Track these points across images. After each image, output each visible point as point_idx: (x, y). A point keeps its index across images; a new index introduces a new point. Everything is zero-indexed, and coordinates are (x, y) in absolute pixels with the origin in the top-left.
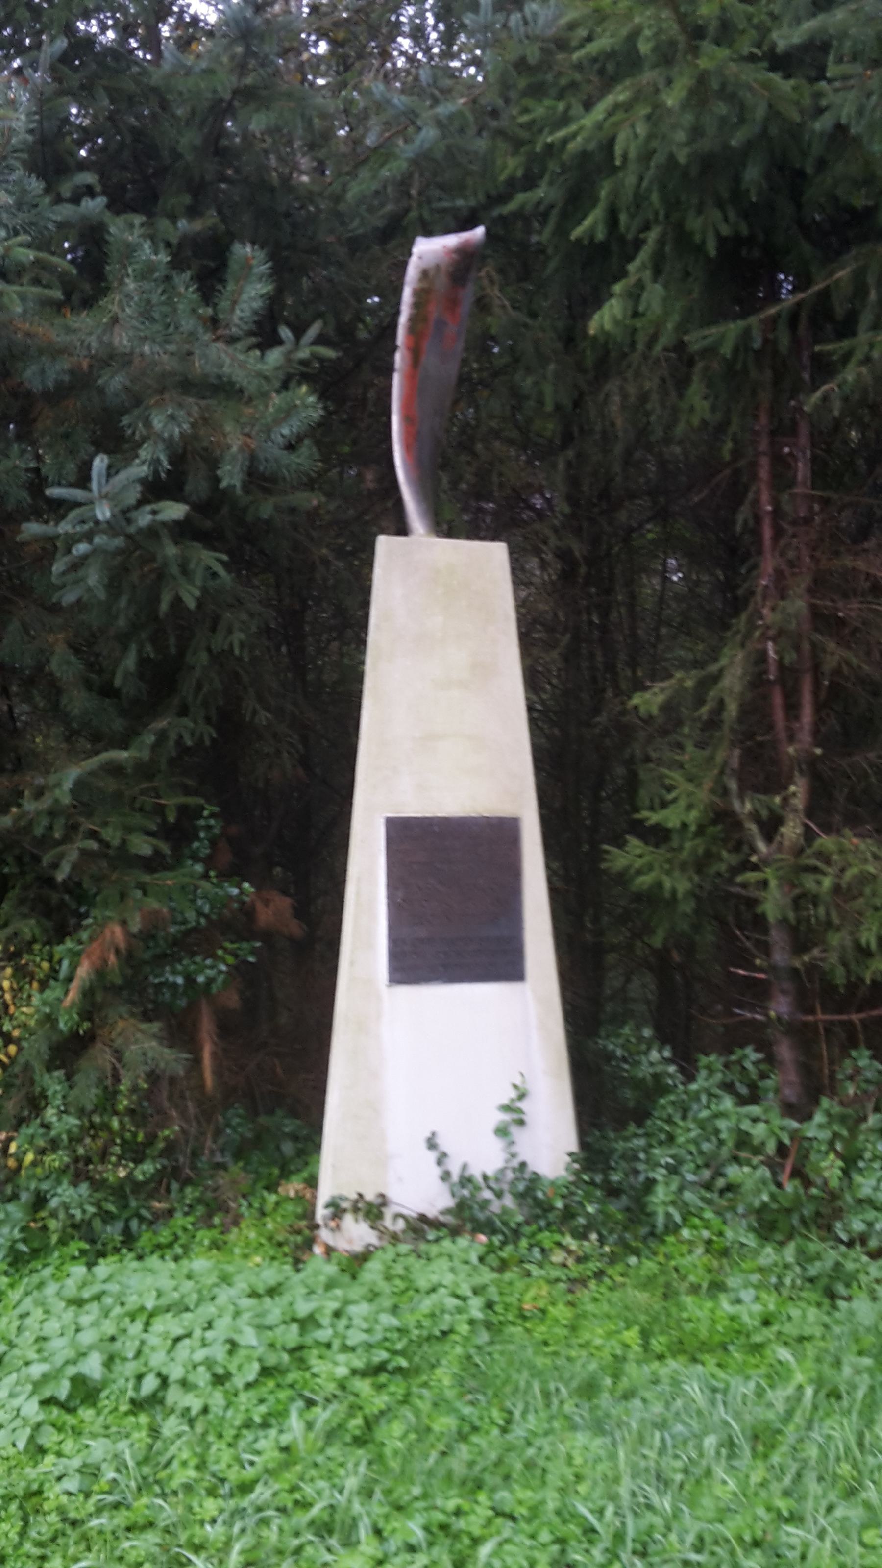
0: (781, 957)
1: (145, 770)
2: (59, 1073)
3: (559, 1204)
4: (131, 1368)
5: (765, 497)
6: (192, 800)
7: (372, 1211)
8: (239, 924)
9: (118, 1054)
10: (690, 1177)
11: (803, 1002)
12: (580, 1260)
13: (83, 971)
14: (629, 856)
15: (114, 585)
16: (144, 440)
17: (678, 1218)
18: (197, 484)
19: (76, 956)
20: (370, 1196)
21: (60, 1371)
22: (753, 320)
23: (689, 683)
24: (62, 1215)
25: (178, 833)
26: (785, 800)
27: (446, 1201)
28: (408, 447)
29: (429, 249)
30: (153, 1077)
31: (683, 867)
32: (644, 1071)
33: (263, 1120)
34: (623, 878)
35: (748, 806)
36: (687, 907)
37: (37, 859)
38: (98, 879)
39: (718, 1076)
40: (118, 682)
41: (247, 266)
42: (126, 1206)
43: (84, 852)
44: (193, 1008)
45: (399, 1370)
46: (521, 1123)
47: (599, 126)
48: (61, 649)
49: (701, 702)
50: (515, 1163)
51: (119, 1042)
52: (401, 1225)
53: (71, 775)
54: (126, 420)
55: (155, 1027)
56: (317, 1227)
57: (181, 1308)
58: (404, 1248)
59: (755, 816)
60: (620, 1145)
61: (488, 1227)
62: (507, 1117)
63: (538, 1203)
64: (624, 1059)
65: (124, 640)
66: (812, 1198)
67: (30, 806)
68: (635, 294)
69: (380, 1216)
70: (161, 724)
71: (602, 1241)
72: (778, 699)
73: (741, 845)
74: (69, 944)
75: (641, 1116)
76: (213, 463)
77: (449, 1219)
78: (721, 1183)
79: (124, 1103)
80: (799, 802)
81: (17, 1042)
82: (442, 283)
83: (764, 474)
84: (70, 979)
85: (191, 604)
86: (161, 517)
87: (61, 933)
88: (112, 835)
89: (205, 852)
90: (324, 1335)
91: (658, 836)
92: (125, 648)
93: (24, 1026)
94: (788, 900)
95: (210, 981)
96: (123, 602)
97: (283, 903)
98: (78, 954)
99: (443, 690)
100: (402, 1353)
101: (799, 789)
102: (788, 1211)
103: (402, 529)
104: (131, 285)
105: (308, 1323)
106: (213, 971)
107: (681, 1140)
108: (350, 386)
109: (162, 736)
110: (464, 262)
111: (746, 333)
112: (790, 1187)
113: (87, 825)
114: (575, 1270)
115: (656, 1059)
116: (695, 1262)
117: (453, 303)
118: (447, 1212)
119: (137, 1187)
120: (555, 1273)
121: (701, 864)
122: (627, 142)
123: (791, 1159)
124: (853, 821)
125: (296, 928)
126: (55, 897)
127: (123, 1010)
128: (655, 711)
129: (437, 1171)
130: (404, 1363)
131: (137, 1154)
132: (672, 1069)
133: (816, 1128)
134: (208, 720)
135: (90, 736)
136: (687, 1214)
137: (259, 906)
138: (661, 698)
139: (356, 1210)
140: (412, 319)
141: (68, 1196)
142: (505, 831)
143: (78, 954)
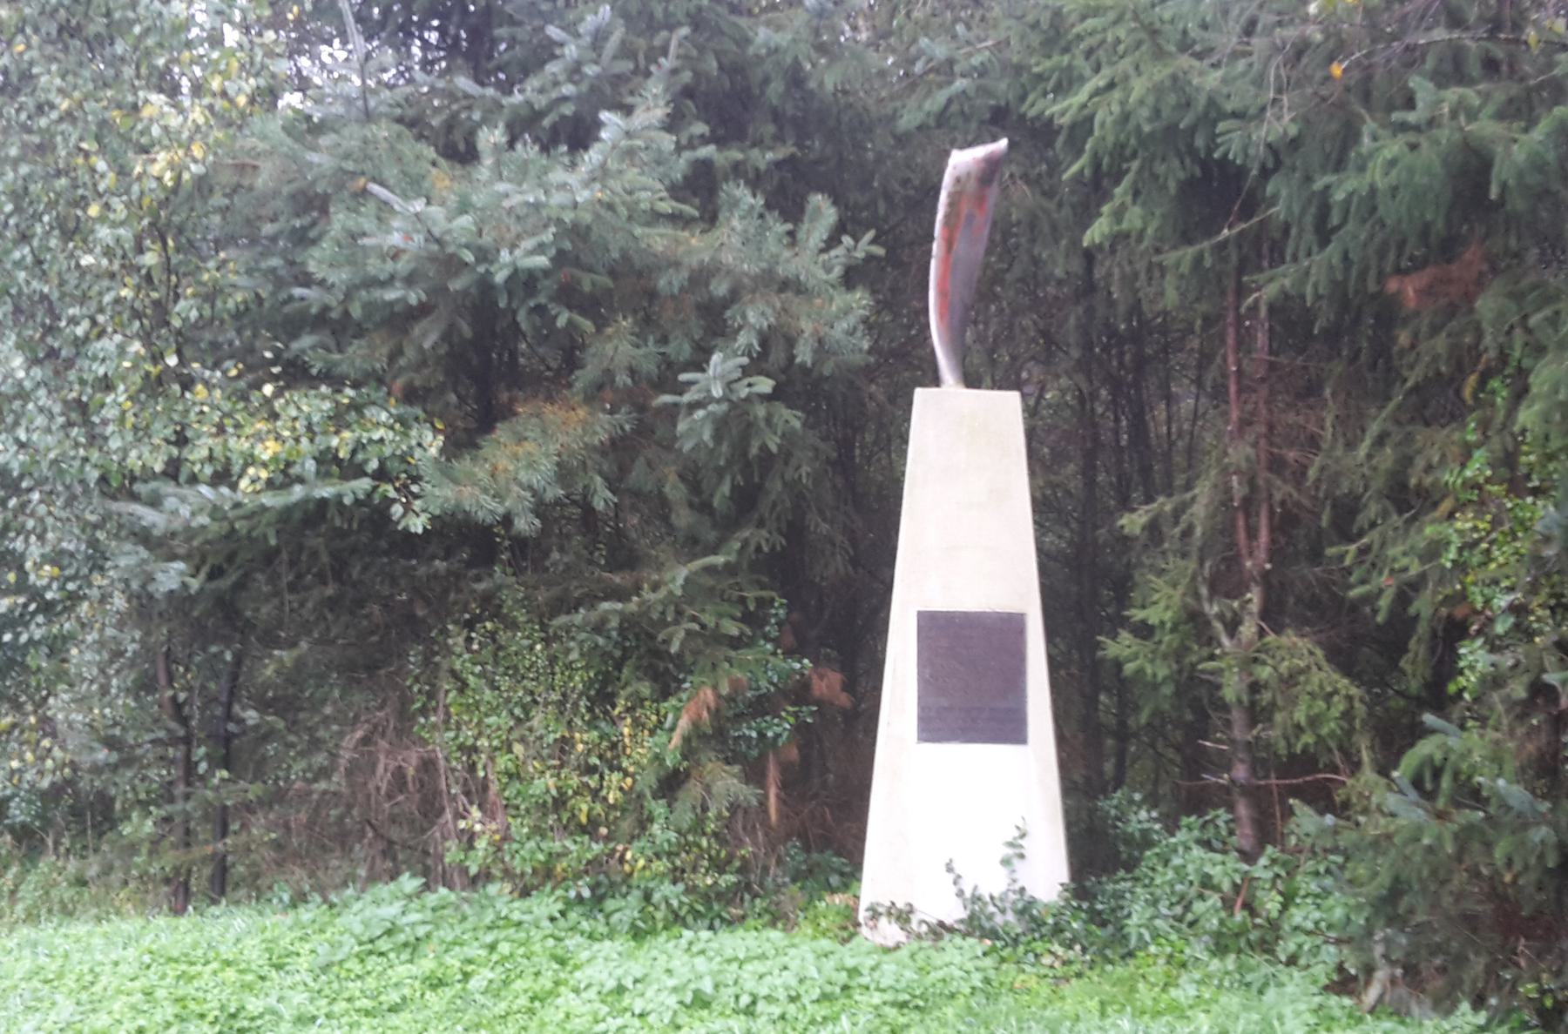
0: (1238, 733)
2: (662, 802)
3: (1050, 921)
4: (732, 991)
5: (1231, 359)
6: (764, 593)
7: (902, 917)
8: (800, 692)
9: (708, 788)
10: (1164, 911)
12: (1064, 963)
13: (684, 723)
14: (1119, 646)
15: (718, 437)
16: (740, 328)
17: (1147, 937)
18: (777, 356)
19: (678, 710)
20: (900, 905)
23: (1168, 508)
26: (1242, 607)
27: (964, 915)
28: (941, 316)
29: (963, 160)
30: (734, 808)
31: (1165, 657)
32: (1133, 827)
33: (815, 856)
34: (1118, 664)
35: (1216, 609)
36: (1168, 690)
37: (652, 637)
39: (1196, 833)
40: (716, 503)
41: (818, 210)
42: (710, 908)
44: (763, 757)
45: (917, 1007)
47: (1084, 106)
48: (673, 478)
50: (1017, 887)
51: (708, 779)
52: (924, 928)
54: (728, 313)
55: (736, 769)
57: (763, 957)
58: (926, 944)
59: (1221, 617)
60: (1110, 887)
61: (993, 934)
62: (1010, 851)
63: (1033, 919)
65: (720, 473)
66: (1256, 926)
68: (1118, 215)
69: (908, 920)
70: (746, 533)
71: (1084, 950)
72: (1241, 523)
73: (1212, 641)
74: (673, 701)
75: (1131, 865)
76: (791, 342)
78: (1190, 917)
79: (711, 827)
80: (1255, 607)
81: (632, 776)
82: (972, 186)
83: (1230, 340)
84: (672, 729)
85: (774, 449)
86: (756, 389)
87: (665, 694)
88: (709, 619)
90: (865, 980)
91: (1144, 631)
93: (636, 763)
94: (1244, 686)
95: (778, 736)
99: (967, 510)
100: (921, 997)
101: (1254, 596)
102: (1237, 935)
103: (936, 381)
104: (735, 223)
105: (854, 972)
106: (780, 727)
108: (892, 278)
110: (991, 168)
112: (1240, 916)
113: (690, 612)
115: (1142, 818)
116: (1159, 970)
117: (980, 200)
118: (962, 921)
119: (720, 896)
120: (1043, 971)
121: (1180, 654)
123: (1242, 896)
124: (1301, 623)
125: (844, 700)
126: (661, 666)
127: (712, 755)
128: (1137, 531)
129: (954, 889)
131: (720, 867)
132: (1157, 827)
133: (1261, 870)
135: (693, 546)
136: (1156, 935)
137: (815, 680)
139: (889, 914)
140: (947, 217)
141: (668, 891)
142: (1013, 625)
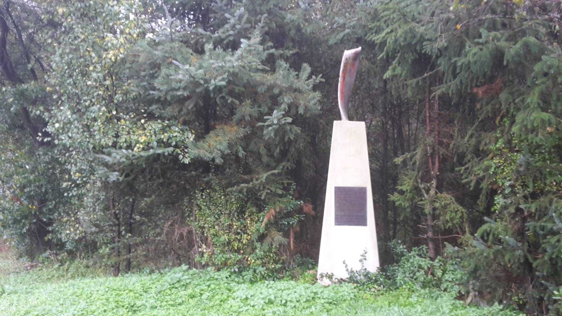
0: (429, 223)
1: (279, 174)
2: (259, 243)
3: (374, 278)
4: (280, 299)
5: (427, 112)
6: (290, 181)
7: (330, 277)
8: (300, 211)
9: (273, 239)
10: (408, 275)
11: (435, 232)
13: (266, 220)
14: (394, 197)
15: (276, 135)
16: (282, 103)
17: (402, 283)
18: (293, 111)
20: (329, 273)
21: (266, 297)
22: (420, 78)
23: (409, 156)
24: (259, 274)
25: (286, 189)
28: (342, 99)
29: (348, 53)
30: (280, 245)
31: (408, 200)
34: (394, 202)
37: (256, 194)
38: (269, 199)
40: (275, 155)
42: (273, 274)
43: (267, 193)
44: (289, 230)
45: (334, 304)
46: (365, 259)
47: (384, 37)
48: (262, 147)
49: (411, 161)
50: (364, 268)
51: (273, 236)
52: (337, 280)
53: (265, 175)
54: (279, 99)
55: (281, 233)
56: (317, 279)
57: (289, 289)
58: (337, 285)
59: (424, 188)
60: (391, 268)
61: (357, 282)
62: (362, 258)
63: (369, 278)
64: (394, 248)
65: (276, 146)
66: (435, 280)
67: (255, 182)
68: (394, 70)
69: (332, 278)
70: (284, 164)
71: (384, 287)
72: (430, 161)
73: (422, 195)
74: (262, 213)
76: (297, 107)
77: (348, 280)
78: (415, 277)
79: (274, 250)
80: (434, 185)
81: (250, 235)
82: (351, 61)
83: (427, 106)
84: (262, 222)
85: (292, 139)
87: (260, 211)
88: (273, 189)
89: (292, 193)
90: (319, 296)
91: (402, 192)
92: (276, 147)
95: (293, 223)
96: (278, 138)
97: (310, 206)
98: (264, 216)
100: (336, 301)
101: (434, 182)
103: (340, 119)
104: (281, 72)
105: (316, 293)
106: (294, 221)
107: (406, 266)
108: (327, 88)
109: (284, 167)
111: (418, 83)
113: (268, 187)
114: (377, 293)
115: (401, 248)
117: (353, 65)
118: (348, 278)
119: (276, 271)
120: (372, 293)
121: (412, 199)
122: (390, 40)
123: (431, 271)
125: (313, 213)
127: (274, 229)
128: (400, 163)
130: (336, 303)
131: (276, 262)
132: (405, 250)
133: (436, 263)
134: (294, 163)
135: (268, 167)
138: (401, 160)
139: (326, 276)
140: (343, 70)
141: (261, 269)
142: (363, 191)
143: (264, 216)
